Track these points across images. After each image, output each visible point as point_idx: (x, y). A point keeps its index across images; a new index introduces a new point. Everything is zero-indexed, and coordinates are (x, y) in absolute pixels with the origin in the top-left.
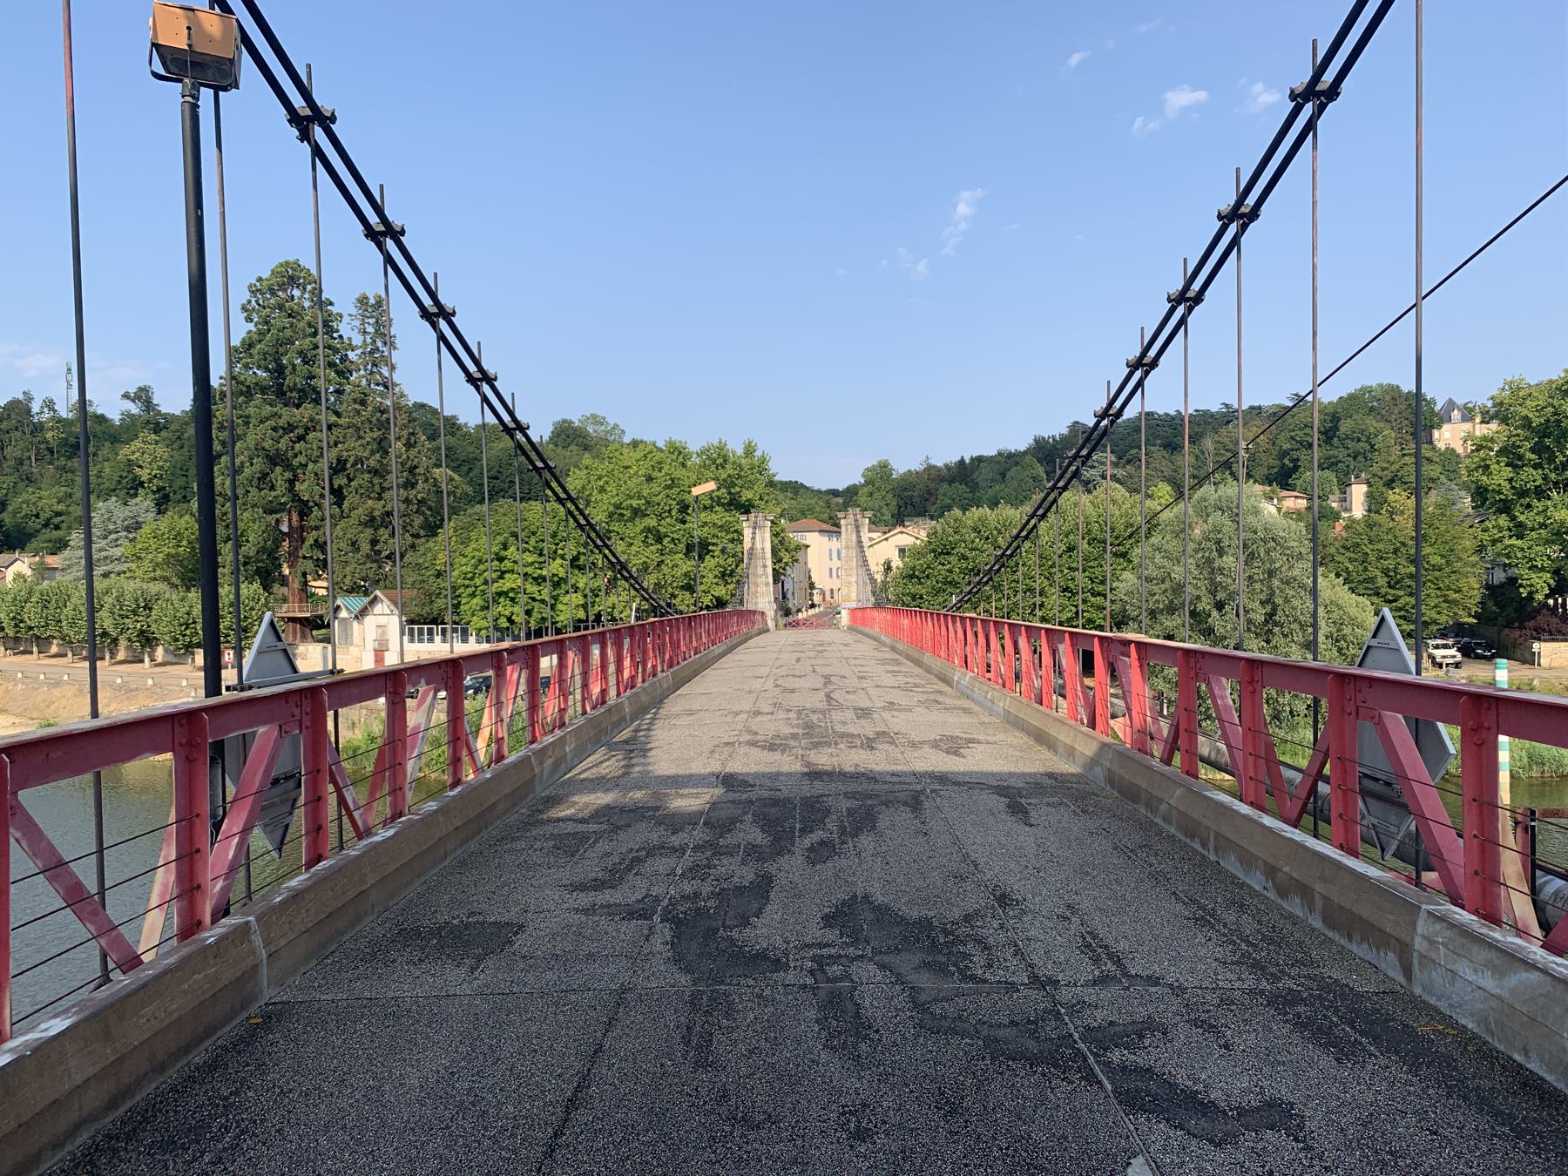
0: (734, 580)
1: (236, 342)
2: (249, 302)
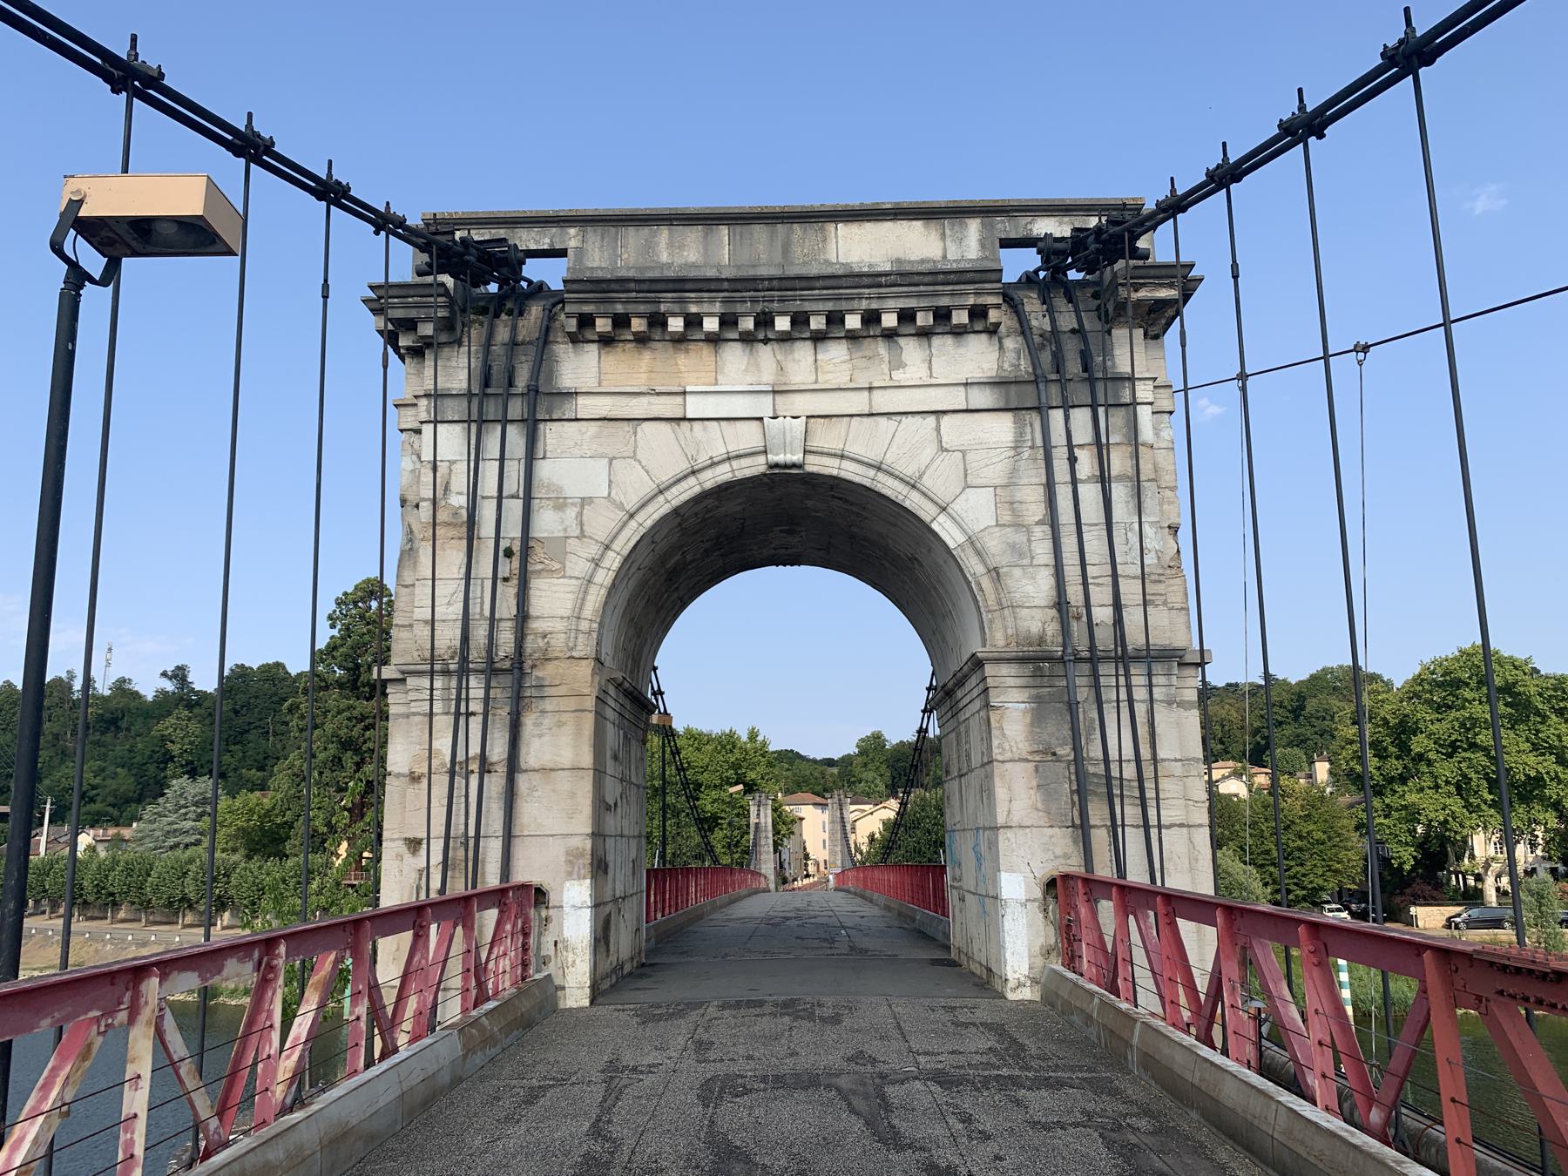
0: (739, 850)
1: (321, 644)
2: (335, 611)
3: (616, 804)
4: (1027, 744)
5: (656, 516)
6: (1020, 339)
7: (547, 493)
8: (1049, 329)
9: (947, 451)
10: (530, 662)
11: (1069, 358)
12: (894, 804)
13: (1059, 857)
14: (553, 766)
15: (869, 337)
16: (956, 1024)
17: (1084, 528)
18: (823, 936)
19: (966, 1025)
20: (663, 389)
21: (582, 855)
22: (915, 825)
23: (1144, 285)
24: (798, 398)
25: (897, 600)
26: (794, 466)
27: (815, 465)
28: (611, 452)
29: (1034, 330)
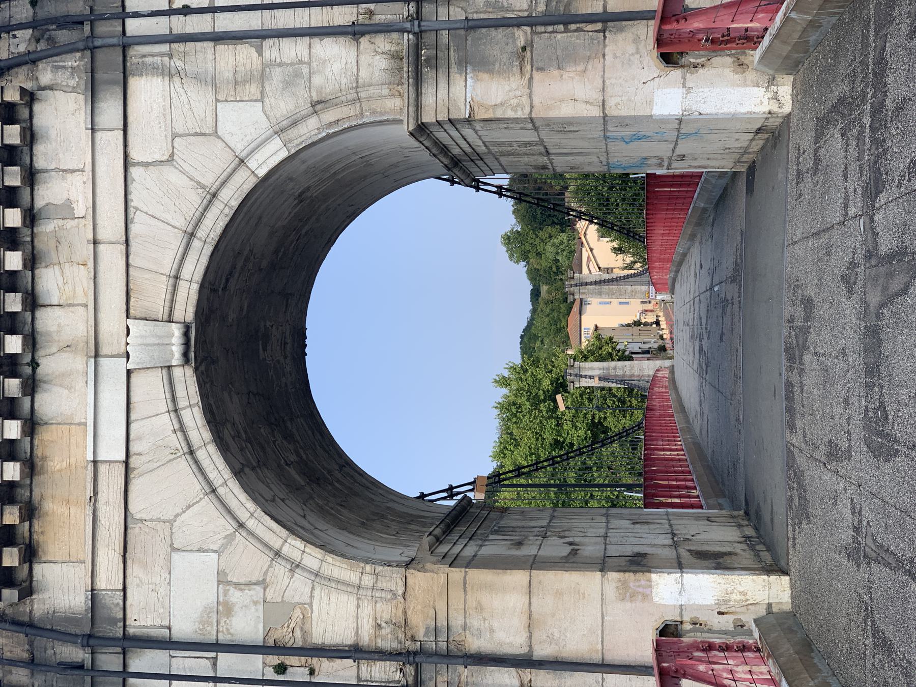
3: (571, 544)
4: (512, 79)
5: (243, 496)
6: (41, 65)
8: (31, 31)
9: (172, 155)
10: (408, 643)
11: (65, 9)
12: (581, 225)
13: (638, 49)
14: (526, 616)
15: (32, 241)
16: (816, 170)
18: (720, 310)
19: (817, 160)
20: (90, 487)
21: (625, 583)
22: (604, 202)
24: (104, 327)
25: (348, 217)
26: (186, 334)
27: (186, 309)
28: (164, 549)
29: (32, 48)
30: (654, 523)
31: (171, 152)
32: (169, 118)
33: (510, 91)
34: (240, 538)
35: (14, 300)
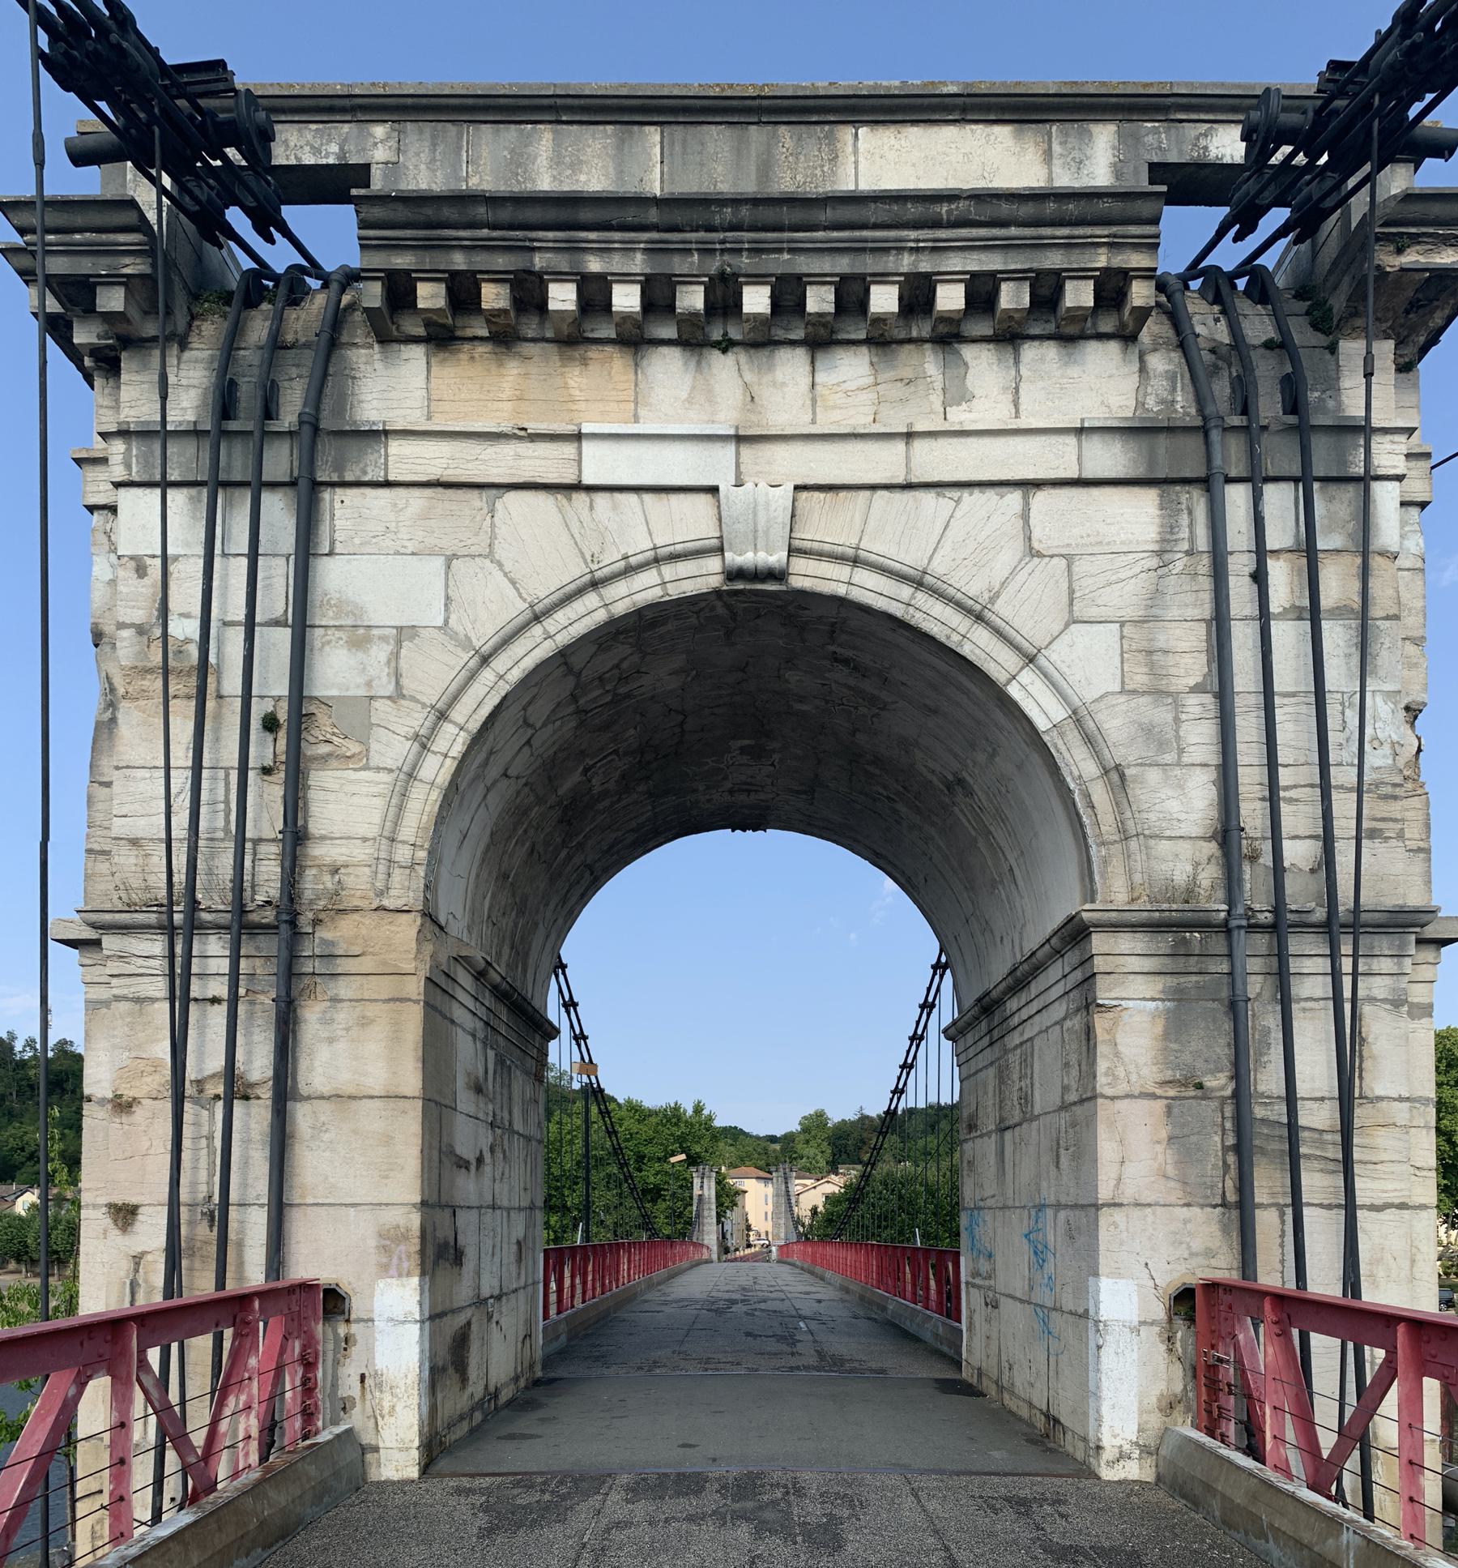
3: (480, 1160)
4: (1155, 1069)
5: (529, 663)
6: (1176, 356)
7: (337, 616)
9: (1040, 555)
10: (310, 915)
15: (910, 341)
17: (1277, 700)
21: (405, 1237)
23: (1415, 239)
24: (780, 451)
25: (909, 880)
27: (808, 576)
28: (450, 544)
30: (519, 1268)
31: (1045, 553)
32: (1096, 550)
33: (1137, 1066)
34: (463, 658)
35: (823, 300)
